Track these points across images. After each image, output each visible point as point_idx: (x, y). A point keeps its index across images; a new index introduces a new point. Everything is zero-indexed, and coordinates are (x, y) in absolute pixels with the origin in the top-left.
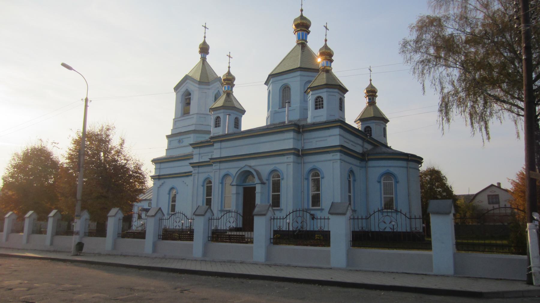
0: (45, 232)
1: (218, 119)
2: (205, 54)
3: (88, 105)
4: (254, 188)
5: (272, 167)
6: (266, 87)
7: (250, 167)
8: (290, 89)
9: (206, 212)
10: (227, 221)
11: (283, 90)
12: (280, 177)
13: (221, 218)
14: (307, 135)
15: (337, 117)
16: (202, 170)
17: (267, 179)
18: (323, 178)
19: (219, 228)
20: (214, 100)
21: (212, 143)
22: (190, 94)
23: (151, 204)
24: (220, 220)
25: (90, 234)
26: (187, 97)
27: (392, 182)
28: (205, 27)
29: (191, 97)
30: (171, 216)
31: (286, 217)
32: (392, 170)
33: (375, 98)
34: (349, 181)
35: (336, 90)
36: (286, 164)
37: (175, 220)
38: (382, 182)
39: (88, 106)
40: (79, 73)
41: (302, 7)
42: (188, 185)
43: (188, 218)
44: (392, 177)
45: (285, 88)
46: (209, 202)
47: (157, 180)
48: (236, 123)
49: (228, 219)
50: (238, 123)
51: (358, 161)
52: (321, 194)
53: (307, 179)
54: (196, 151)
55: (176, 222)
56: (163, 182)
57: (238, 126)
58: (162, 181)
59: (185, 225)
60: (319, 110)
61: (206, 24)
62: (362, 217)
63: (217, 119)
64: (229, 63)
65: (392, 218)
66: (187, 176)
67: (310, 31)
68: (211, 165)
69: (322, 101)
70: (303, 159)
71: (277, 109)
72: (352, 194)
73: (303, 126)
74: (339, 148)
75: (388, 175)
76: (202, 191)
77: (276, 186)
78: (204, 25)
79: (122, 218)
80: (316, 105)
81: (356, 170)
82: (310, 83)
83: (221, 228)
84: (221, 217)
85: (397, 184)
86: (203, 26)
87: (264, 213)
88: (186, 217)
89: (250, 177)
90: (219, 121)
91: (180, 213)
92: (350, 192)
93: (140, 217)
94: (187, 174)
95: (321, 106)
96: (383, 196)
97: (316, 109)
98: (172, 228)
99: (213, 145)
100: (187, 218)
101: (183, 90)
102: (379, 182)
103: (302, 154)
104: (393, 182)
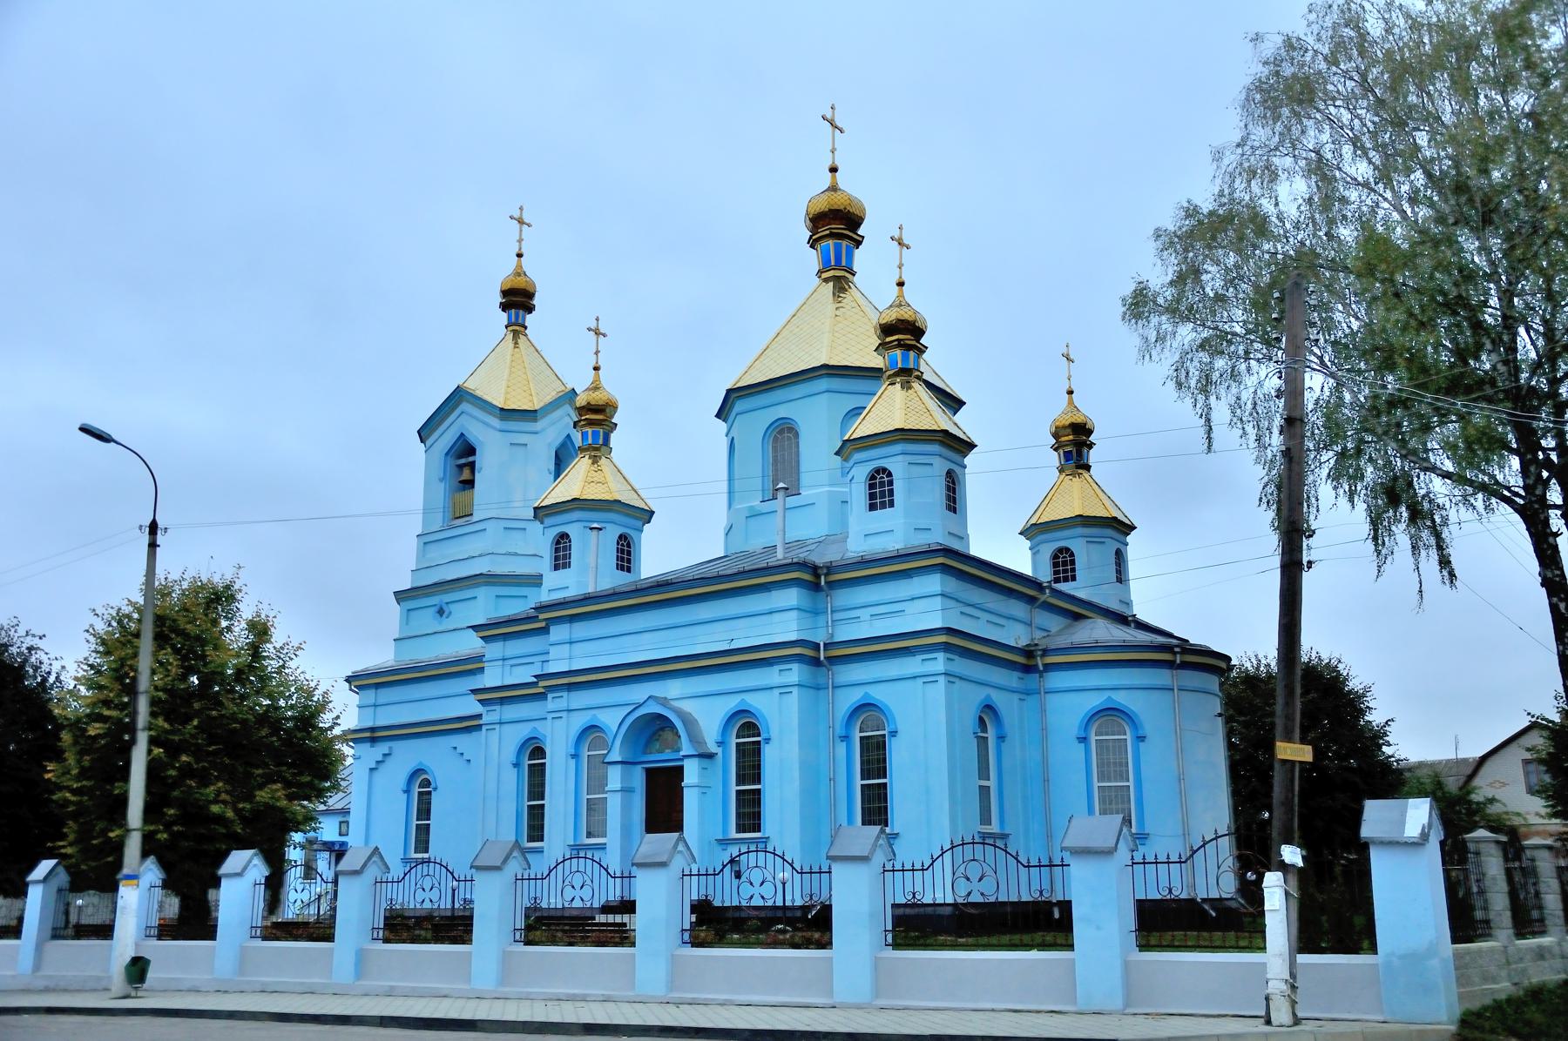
1: (562, 541)
2: (521, 312)
3: (158, 543)
4: (679, 770)
5: (732, 703)
6: (722, 426)
7: (664, 702)
8: (797, 435)
9: (505, 861)
10: (566, 883)
11: (775, 440)
12: (759, 735)
14: (844, 597)
15: (937, 538)
16: (511, 712)
17: (720, 739)
18: (894, 733)
19: (544, 905)
20: (552, 468)
21: (543, 624)
22: (471, 451)
23: (348, 827)
25: (167, 931)
26: (463, 461)
27: (1124, 737)
28: (521, 222)
29: (478, 458)
30: (413, 865)
31: (556, 867)
32: (1121, 699)
33: (1085, 450)
34: (982, 742)
35: (936, 448)
36: (776, 692)
37: (420, 882)
38: (1093, 738)
39: (159, 546)
40: (130, 450)
41: (834, 158)
42: (469, 761)
43: (325, 879)
44: (1121, 721)
45: (781, 432)
46: (536, 818)
47: (369, 744)
48: (622, 551)
50: (629, 553)
51: (1016, 674)
52: (891, 784)
53: (846, 738)
54: (494, 650)
55: (424, 890)
56: (387, 752)
57: (629, 561)
58: (383, 748)
59: (462, 896)
61: (521, 209)
62: (811, 869)
63: (558, 543)
64: (597, 353)
65: (986, 868)
66: (468, 730)
68: (541, 696)
69: (891, 483)
70: (833, 675)
71: (756, 503)
72: (992, 783)
73: (830, 569)
74: (942, 639)
75: (1110, 714)
76: (512, 784)
77: (750, 764)
78: (515, 216)
79: (263, 882)
80: (872, 496)
81: (1005, 703)
82: (861, 414)
83: (549, 903)
84: (550, 872)
85: (1141, 744)
86: (511, 217)
87: (664, 859)
88: (452, 874)
89: (668, 735)
90: (565, 549)
91: (435, 863)
92: (984, 772)
93: (310, 872)
94: (469, 725)
95: (878, 501)
96: (1096, 784)
97: (872, 507)
98: (412, 906)
99: (545, 631)
101: (445, 438)
102: (1083, 740)
103: (826, 658)
104: (1128, 737)
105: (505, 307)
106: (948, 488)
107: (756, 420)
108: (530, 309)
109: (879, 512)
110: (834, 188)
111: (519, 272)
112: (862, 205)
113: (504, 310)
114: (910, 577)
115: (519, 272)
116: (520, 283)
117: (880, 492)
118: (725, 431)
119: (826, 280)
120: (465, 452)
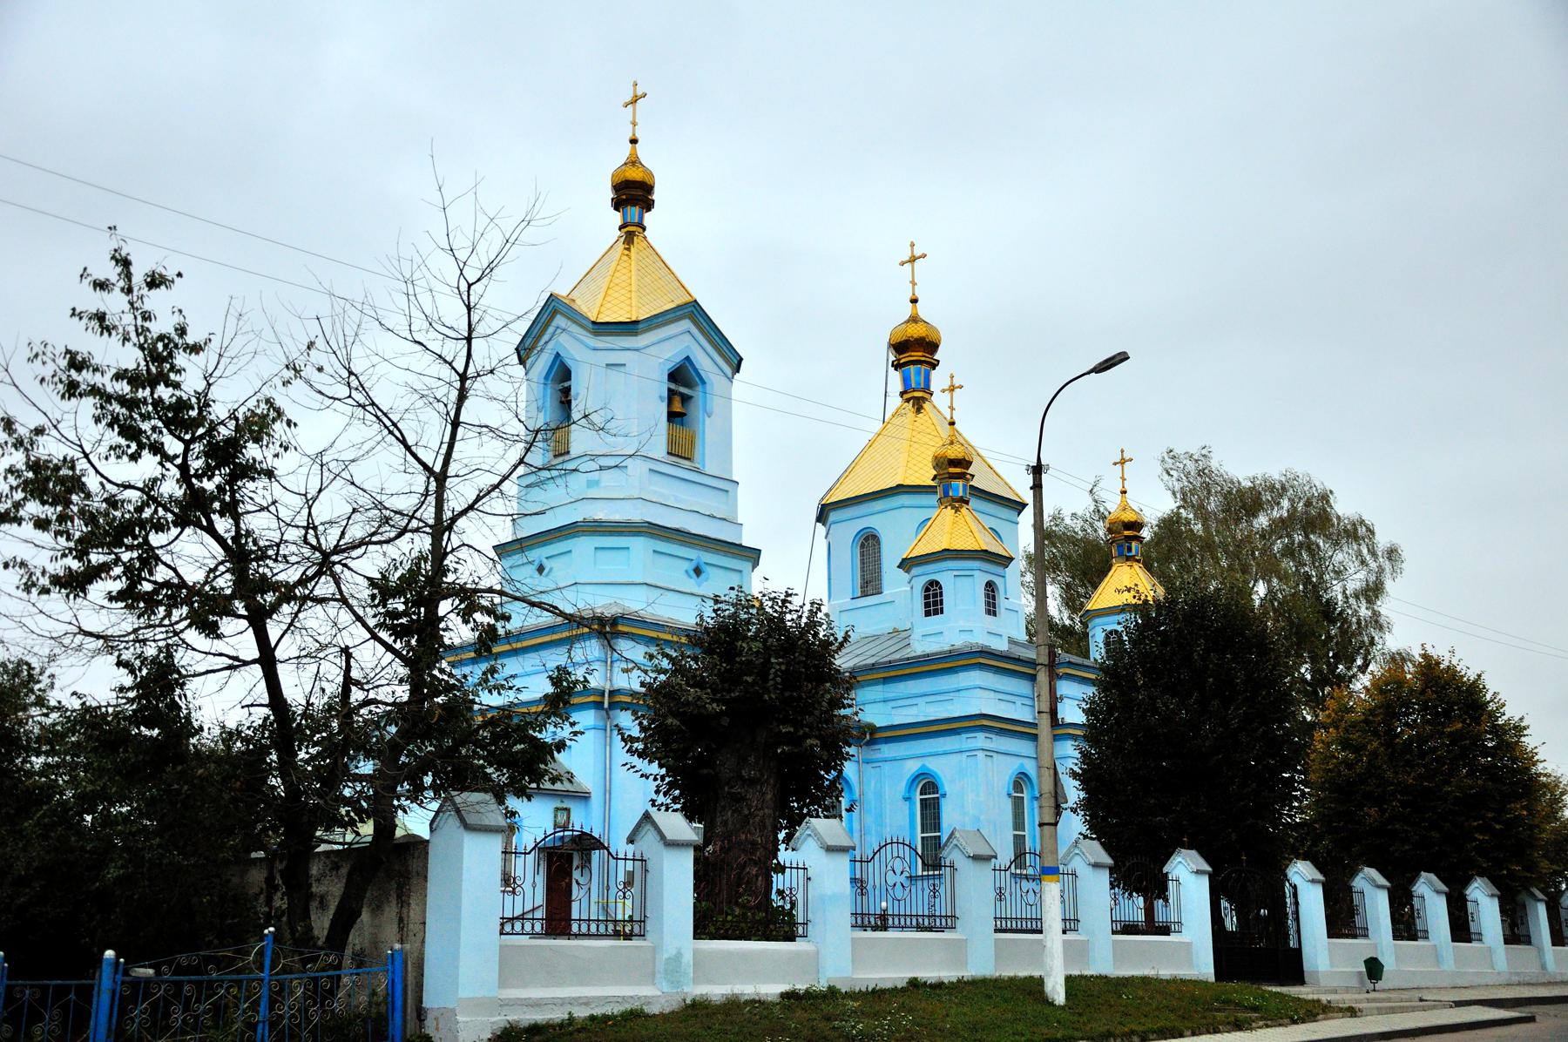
0: (586, 798)
8: (878, 542)
10: (889, 868)
11: (862, 546)
13: (873, 857)
24: (871, 864)
45: (867, 539)
49: (891, 864)
57: (994, 607)
60: (933, 618)
67: (938, 361)
80: (927, 605)
97: (928, 614)
100: (609, 853)
101: (542, 363)
105: (618, 205)
106: (987, 596)
107: (848, 527)
108: (649, 205)
109: (933, 617)
110: (914, 319)
111: (634, 162)
112: (938, 332)
113: (617, 209)
114: (957, 672)
115: (634, 162)
116: (634, 174)
117: (933, 601)
118: (824, 534)
119: (908, 401)
120: (562, 375)
